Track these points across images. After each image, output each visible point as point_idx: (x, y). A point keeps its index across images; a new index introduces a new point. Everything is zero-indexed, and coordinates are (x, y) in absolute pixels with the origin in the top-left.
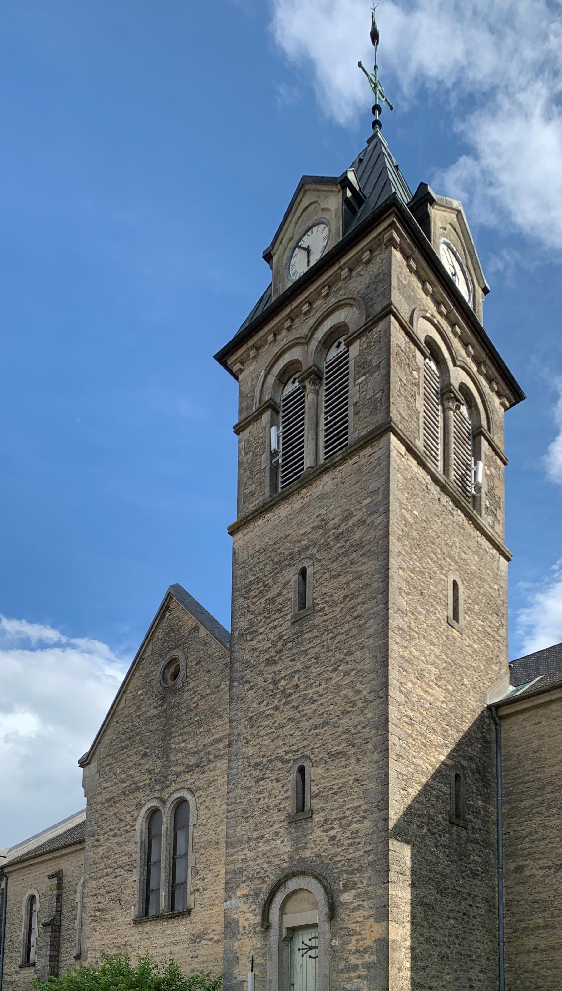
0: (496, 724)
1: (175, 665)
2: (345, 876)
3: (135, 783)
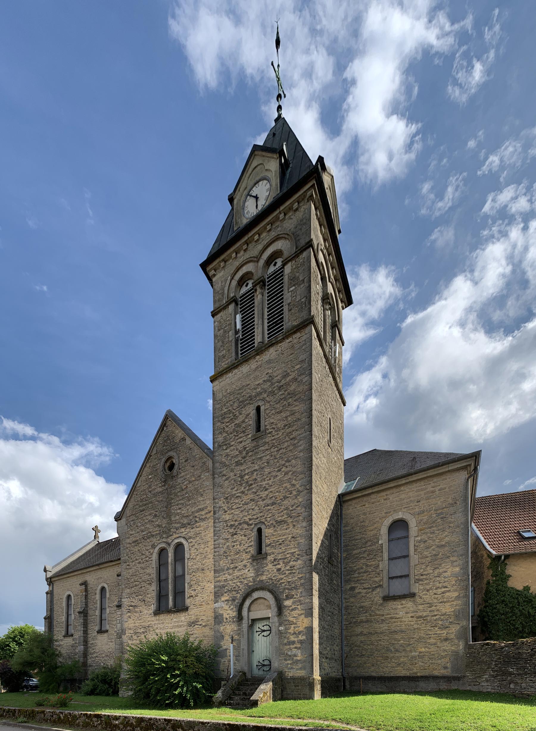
2: (287, 591)
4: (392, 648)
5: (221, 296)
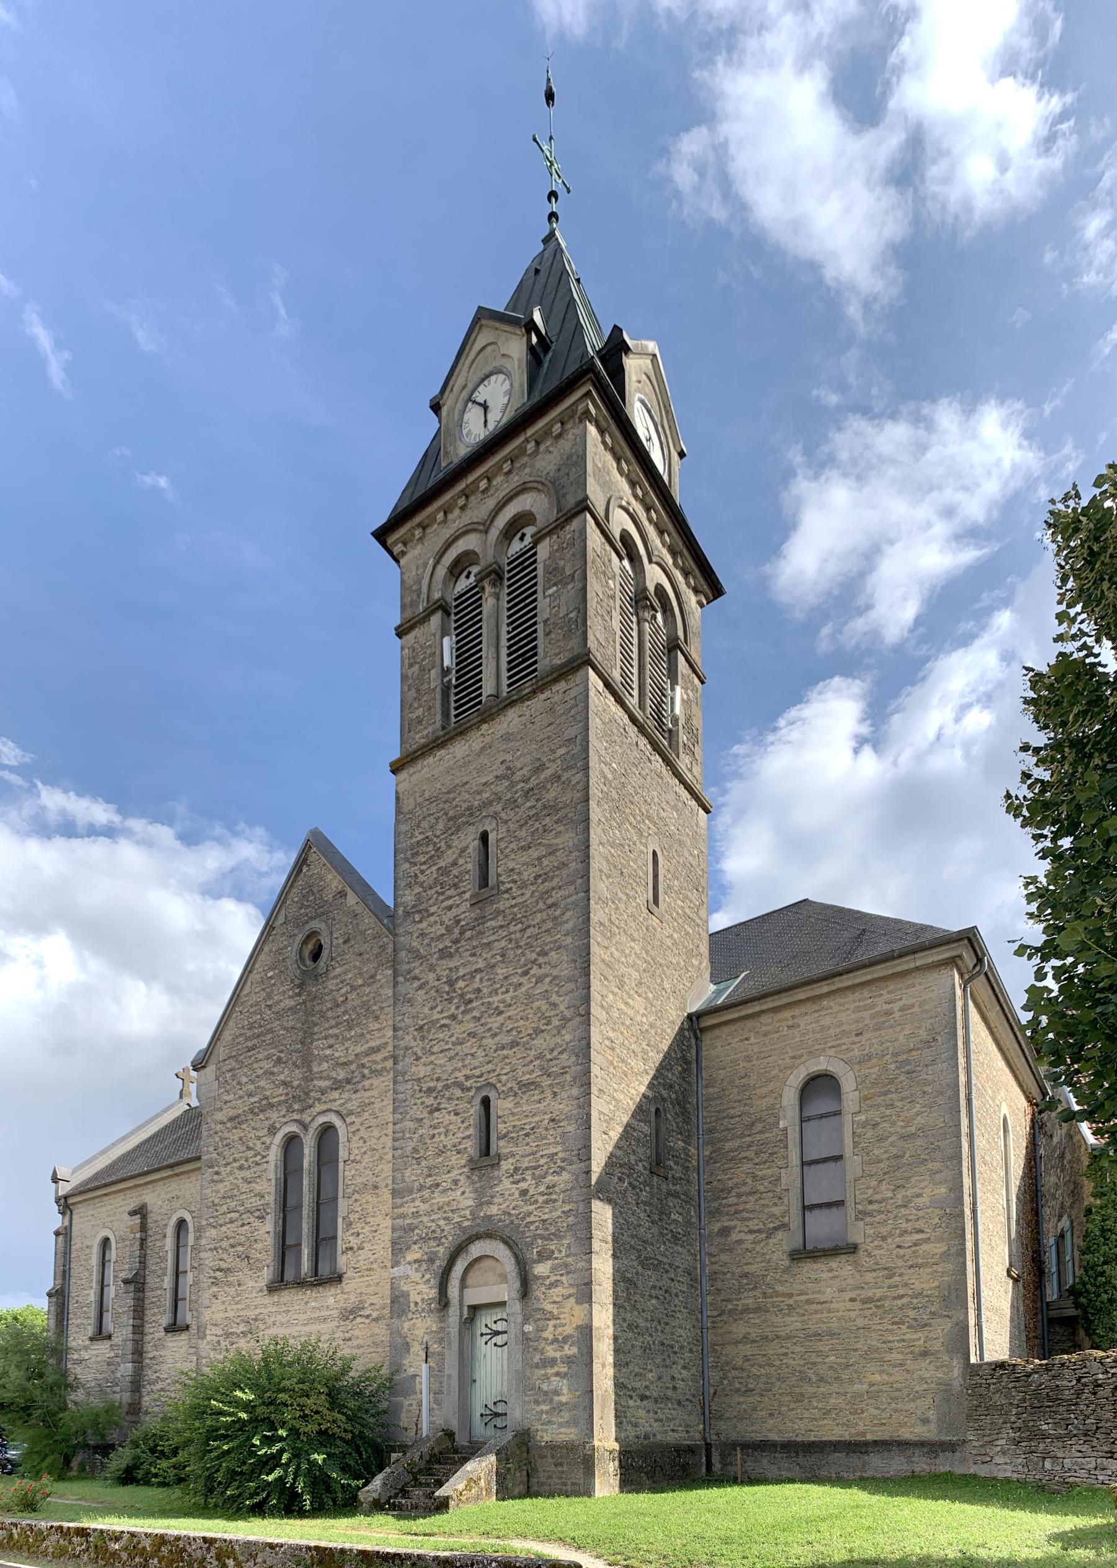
0: (697, 1038)
1: (314, 940)
2: (540, 1241)
3: (267, 1098)
4: (810, 1374)
5: (415, 597)
